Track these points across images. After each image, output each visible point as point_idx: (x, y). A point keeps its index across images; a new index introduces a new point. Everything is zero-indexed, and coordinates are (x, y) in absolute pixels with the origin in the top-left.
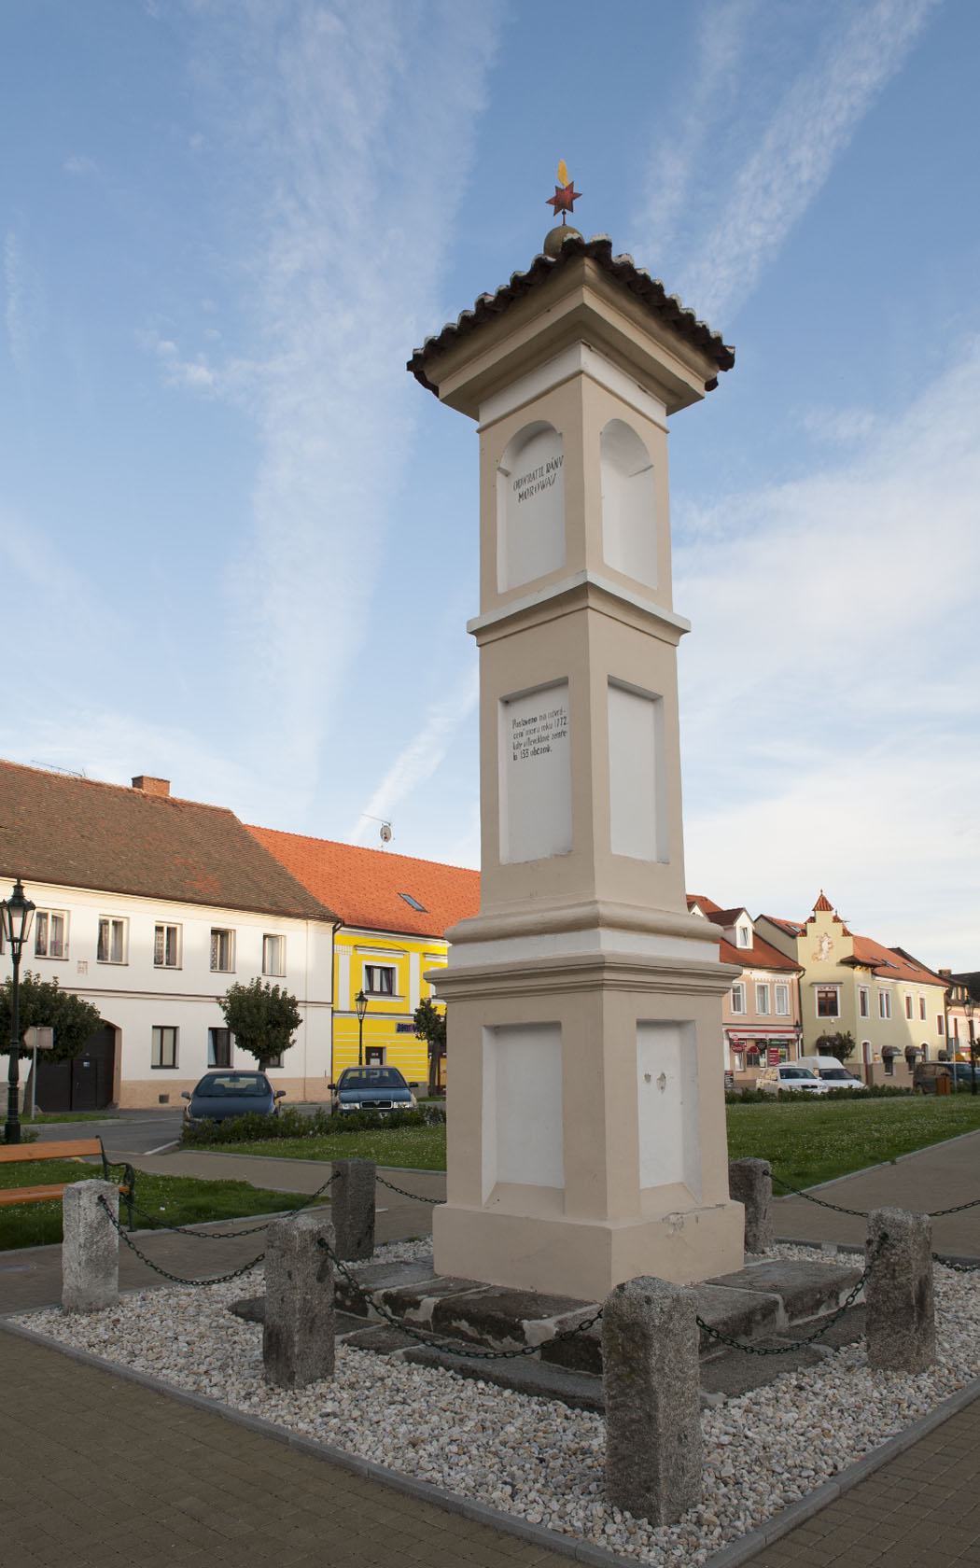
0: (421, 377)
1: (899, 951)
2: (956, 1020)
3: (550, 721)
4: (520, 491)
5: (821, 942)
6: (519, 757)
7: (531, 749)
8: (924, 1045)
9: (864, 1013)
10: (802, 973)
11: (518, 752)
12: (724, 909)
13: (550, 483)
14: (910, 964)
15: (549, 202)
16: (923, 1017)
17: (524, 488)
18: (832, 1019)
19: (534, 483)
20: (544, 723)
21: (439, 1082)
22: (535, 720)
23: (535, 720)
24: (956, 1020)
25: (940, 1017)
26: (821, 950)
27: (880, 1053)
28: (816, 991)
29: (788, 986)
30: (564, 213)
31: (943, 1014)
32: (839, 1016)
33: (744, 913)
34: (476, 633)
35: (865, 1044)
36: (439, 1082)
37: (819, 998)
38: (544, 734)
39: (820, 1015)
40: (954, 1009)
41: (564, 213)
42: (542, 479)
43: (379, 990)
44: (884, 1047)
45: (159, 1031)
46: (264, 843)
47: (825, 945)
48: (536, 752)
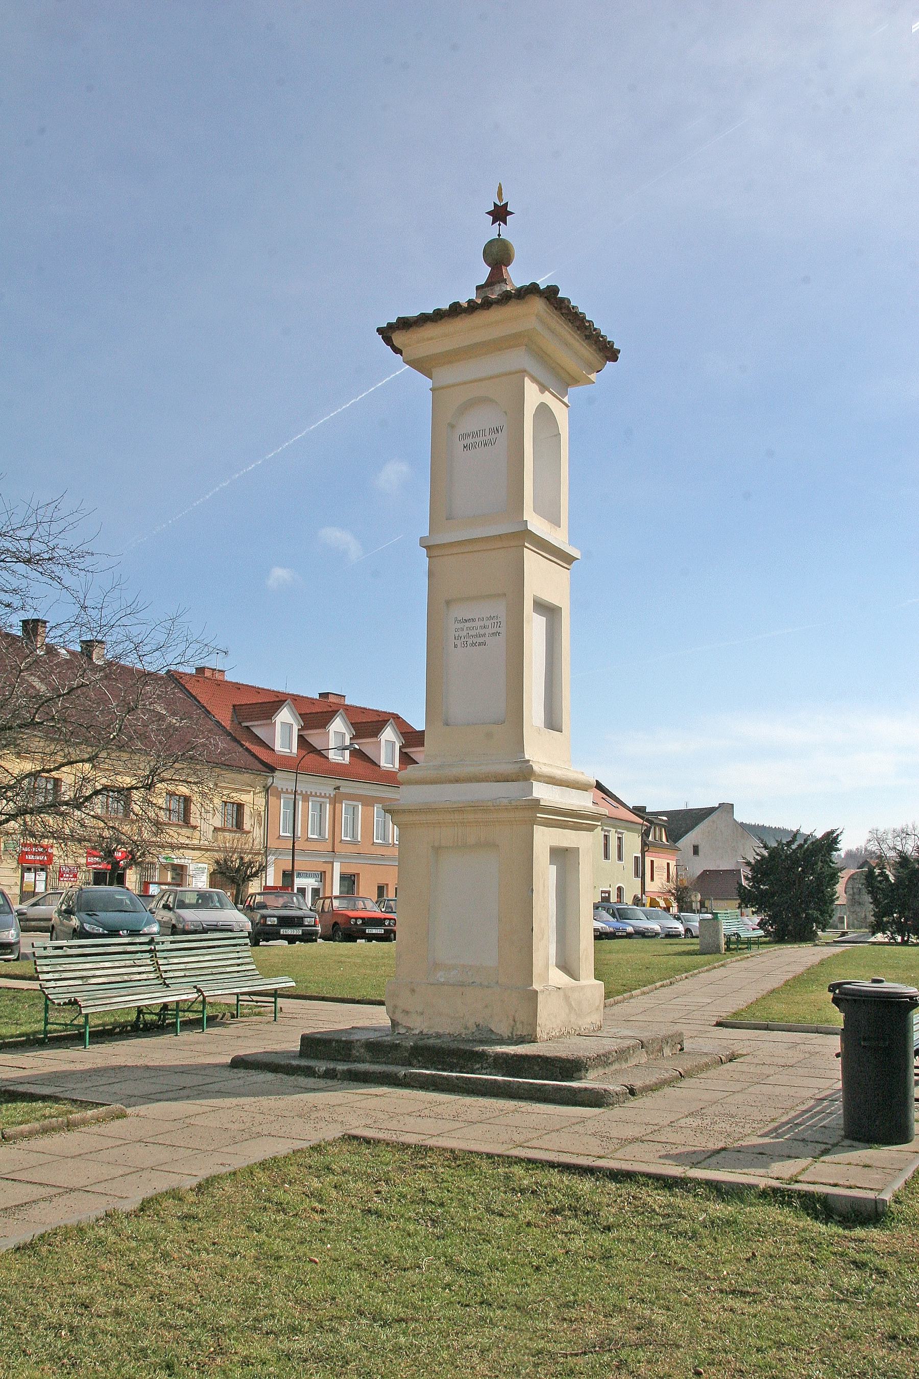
0: (388, 341)
2: (652, 862)
3: (488, 623)
4: (465, 442)
6: (459, 645)
7: (470, 641)
11: (458, 642)
13: (492, 443)
14: (608, 799)
16: (620, 858)
17: (469, 441)
19: (477, 440)
20: (482, 623)
21: (266, 884)
22: (474, 620)
23: (474, 620)
24: (652, 862)
25: (636, 858)
30: (499, 225)
34: (428, 548)
36: (266, 884)
38: (482, 632)
41: (499, 225)
42: (485, 438)
48: (473, 644)
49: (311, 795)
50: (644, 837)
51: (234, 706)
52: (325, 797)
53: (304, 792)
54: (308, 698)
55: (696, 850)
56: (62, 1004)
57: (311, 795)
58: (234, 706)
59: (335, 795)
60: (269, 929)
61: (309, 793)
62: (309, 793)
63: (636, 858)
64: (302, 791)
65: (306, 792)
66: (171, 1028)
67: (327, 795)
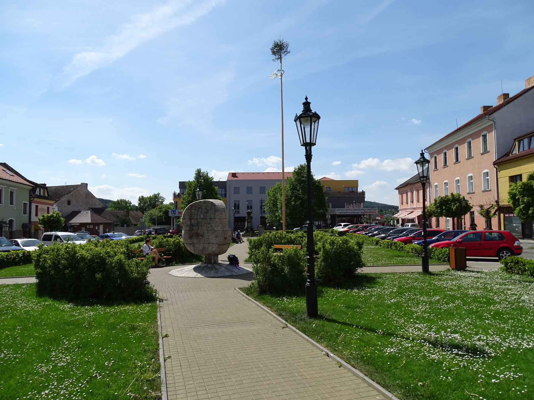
2: (37, 206)
8: (11, 221)
14: (8, 171)
24: (37, 206)
31: (28, 203)
40: (36, 199)
50: (31, 193)
55: (69, 203)
63: (25, 204)
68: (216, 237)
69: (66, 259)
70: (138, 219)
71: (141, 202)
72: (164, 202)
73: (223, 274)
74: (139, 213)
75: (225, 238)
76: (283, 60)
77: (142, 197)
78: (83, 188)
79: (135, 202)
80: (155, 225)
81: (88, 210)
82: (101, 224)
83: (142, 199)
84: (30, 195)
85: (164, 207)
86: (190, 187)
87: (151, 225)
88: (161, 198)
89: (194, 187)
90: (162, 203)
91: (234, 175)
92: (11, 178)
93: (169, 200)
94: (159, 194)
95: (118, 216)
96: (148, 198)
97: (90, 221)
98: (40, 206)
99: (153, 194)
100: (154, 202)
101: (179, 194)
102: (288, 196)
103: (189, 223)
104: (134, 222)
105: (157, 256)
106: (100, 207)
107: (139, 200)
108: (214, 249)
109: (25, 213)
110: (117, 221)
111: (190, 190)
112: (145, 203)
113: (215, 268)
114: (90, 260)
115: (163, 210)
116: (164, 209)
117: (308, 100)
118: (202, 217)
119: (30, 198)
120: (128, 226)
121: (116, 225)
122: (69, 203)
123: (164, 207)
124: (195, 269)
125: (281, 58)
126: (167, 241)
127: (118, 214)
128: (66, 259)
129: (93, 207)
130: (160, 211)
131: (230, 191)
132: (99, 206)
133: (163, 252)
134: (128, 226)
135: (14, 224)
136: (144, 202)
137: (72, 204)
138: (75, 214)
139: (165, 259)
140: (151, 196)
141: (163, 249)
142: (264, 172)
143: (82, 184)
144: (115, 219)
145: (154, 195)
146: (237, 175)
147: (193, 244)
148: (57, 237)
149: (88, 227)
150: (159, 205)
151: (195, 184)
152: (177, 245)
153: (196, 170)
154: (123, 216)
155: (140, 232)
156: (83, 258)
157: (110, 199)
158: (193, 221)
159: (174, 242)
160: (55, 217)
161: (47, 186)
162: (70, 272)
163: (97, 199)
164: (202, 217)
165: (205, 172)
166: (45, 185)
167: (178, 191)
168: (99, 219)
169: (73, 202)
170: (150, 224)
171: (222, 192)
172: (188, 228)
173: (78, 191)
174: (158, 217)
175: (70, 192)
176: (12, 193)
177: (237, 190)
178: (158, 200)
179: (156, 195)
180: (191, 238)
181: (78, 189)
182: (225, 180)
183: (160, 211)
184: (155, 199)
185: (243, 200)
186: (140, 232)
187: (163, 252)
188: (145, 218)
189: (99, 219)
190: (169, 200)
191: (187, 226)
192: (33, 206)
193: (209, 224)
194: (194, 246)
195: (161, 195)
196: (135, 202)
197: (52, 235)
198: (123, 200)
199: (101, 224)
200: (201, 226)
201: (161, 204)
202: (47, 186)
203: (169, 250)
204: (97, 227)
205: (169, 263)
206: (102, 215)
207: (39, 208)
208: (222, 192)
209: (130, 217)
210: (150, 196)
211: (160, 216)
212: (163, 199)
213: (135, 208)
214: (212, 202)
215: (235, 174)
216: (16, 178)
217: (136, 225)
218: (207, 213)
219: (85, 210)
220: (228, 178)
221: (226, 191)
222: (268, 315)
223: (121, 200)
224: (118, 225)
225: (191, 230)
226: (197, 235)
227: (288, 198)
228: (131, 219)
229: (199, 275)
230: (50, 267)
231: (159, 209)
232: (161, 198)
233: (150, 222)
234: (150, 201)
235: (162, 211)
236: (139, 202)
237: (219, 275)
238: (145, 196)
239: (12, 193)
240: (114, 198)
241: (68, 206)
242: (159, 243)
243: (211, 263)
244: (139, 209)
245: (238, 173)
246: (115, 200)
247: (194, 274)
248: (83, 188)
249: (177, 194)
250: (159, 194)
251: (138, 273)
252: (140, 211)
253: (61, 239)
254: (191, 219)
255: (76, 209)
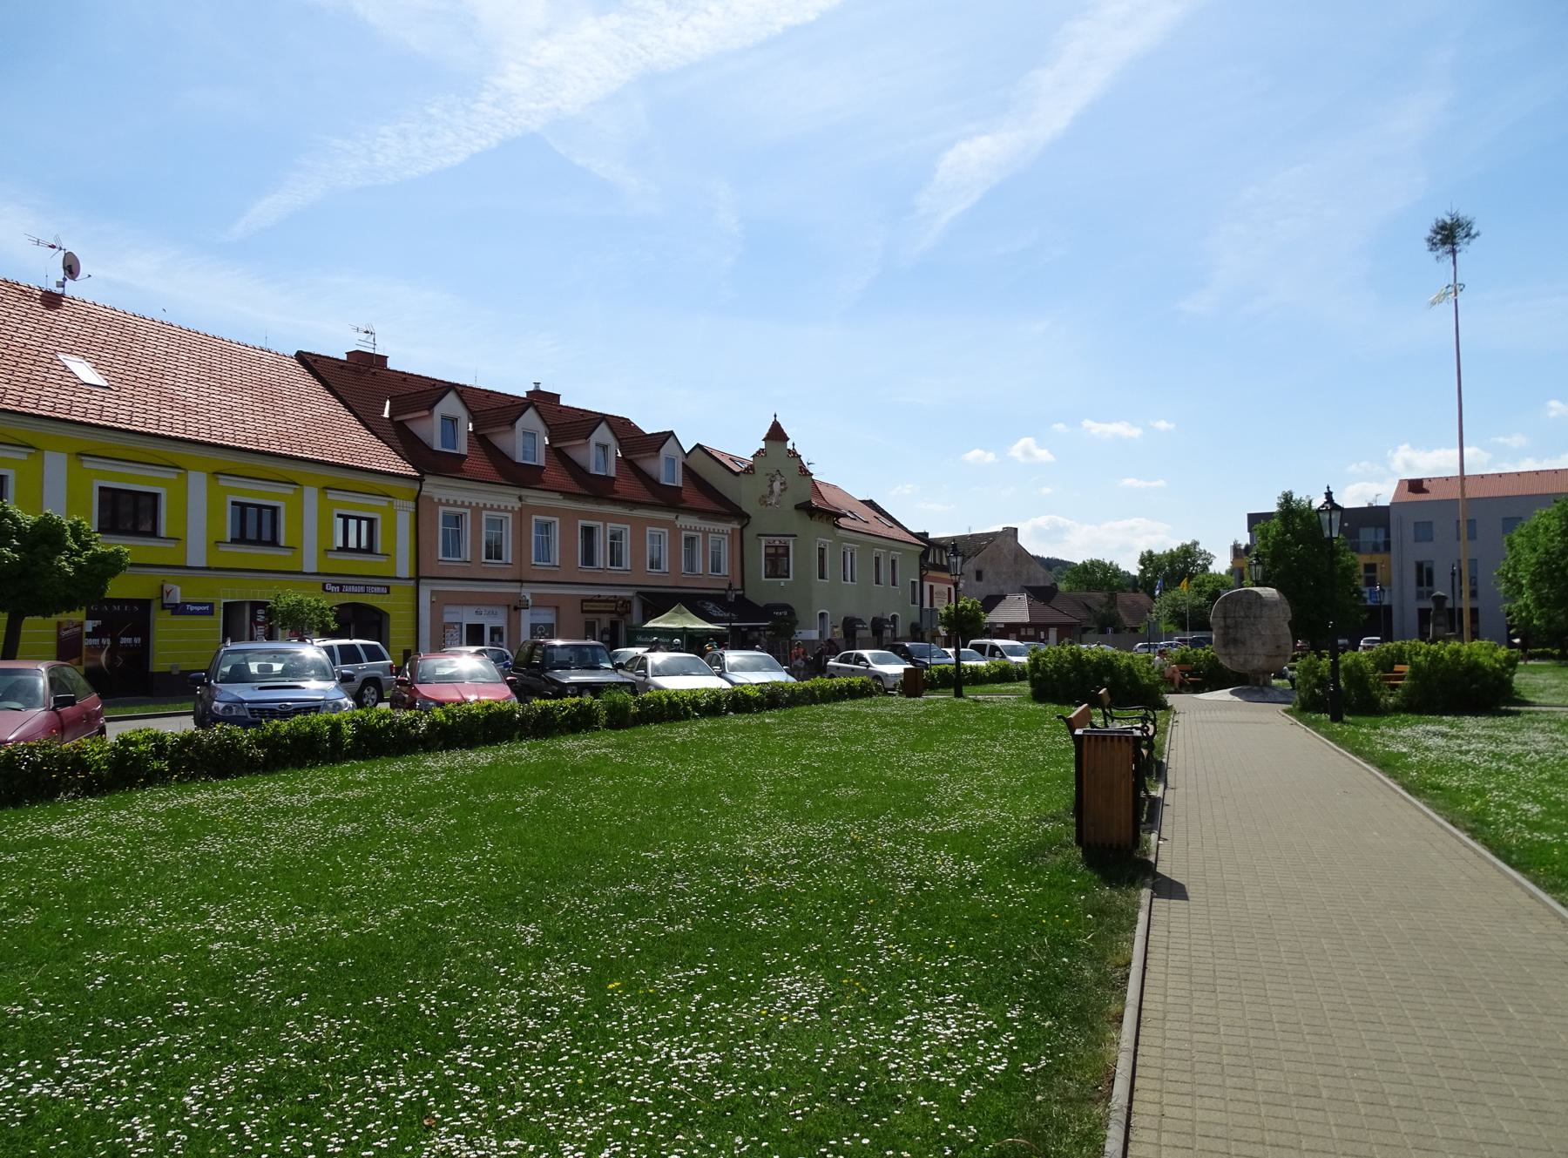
1: (870, 504)
2: (931, 587)
5: (772, 482)
8: (894, 617)
9: (822, 576)
10: (746, 521)
12: (648, 432)
14: (882, 519)
15: (776, 434)
18: (783, 581)
24: (931, 587)
26: (772, 492)
27: (840, 625)
28: (763, 545)
29: (726, 537)
31: (917, 580)
32: (791, 578)
33: (671, 439)
35: (822, 615)
37: (767, 555)
39: (102, 489)
40: (932, 574)
43: (355, 546)
44: (845, 618)
45: (422, 581)
46: (398, 445)
47: (777, 486)
49: (485, 507)
50: (923, 561)
51: (1430, 523)
52: (506, 510)
53: (474, 504)
54: (396, 372)
55: (979, 575)
56: (1053, 633)
57: (485, 507)
58: (1430, 523)
59: (521, 509)
60: (181, 709)
61: (481, 505)
62: (481, 505)
64: (477, 504)
65: (477, 504)
66: (870, 694)
67: (510, 508)
68: (1263, 644)
69: (1070, 663)
70: (1140, 613)
71: (1146, 568)
72: (1210, 567)
73: (1273, 700)
74: (1142, 598)
75: (1278, 647)
76: (1458, 255)
77: (1150, 553)
78: (1008, 539)
79: (1133, 568)
80: (1185, 630)
81: (1021, 592)
82: (1052, 625)
83: (1148, 559)
84: (921, 565)
85: (1209, 582)
86: (1266, 538)
87: (1175, 631)
88: (1201, 554)
89: (1273, 538)
90: (1205, 568)
91: (1416, 486)
92: (896, 536)
93: (1221, 564)
94: (1195, 544)
95: (1088, 608)
96: (1165, 555)
97: (1027, 620)
98: (937, 586)
99: (1179, 545)
100: (1182, 566)
101: (1247, 546)
102: (1553, 553)
103: (1222, 623)
104: (1128, 621)
105: (1178, 677)
106: (1048, 584)
107: (1142, 562)
108: (1261, 663)
109: (914, 603)
110: (1089, 620)
111: (1265, 545)
112: (1158, 569)
113: (1263, 692)
114: (1097, 663)
115: (1206, 589)
116: (1209, 588)
117: (1331, 490)
118: (1242, 614)
119: (921, 573)
120: (1116, 631)
121: (1085, 630)
122: (979, 575)
123: (1209, 582)
124: (1232, 693)
125: (1454, 252)
126: (1195, 654)
127: (1088, 602)
128: (1070, 663)
129: (1032, 584)
130: (1199, 593)
131: (1402, 534)
132: (1043, 579)
133: (1188, 672)
134: (1116, 631)
135: (899, 622)
136: (1154, 568)
137: (985, 578)
138: (991, 602)
139: (1191, 682)
140: (1175, 550)
141: (1188, 667)
142: (1520, 470)
143: (1007, 530)
144: (1083, 615)
145: (1182, 547)
146: (1425, 486)
147: (1229, 655)
148: (994, 648)
149: (1023, 633)
150: (1196, 574)
151: (1277, 531)
152: (1213, 661)
153: (1280, 495)
154: (1101, 606)
155: (1145, 646)
156: (1089, 660)
157: (1060, 557)
158: (1229, 620)
159: (1206, 656)
160: (970, 611)
161: (930, 537)
162: (1075, 676)
163: (1037, 558)
164: (1242, 614)
165: (1304, 498)
166: (926, 534)
167: (1244, 539)
168: (1048, 614)
169: (989, 573)
170: (1171, 627)
171: (1376, 537)
172: (1222, 631)
173: (997, 546)
174: (1193, 608)
175: (980, 550)
176: (893, 562)
177: (1424, 531)
178: (1195, 561)
179: (1187, 546)
180: (1225, 646)
181: (998, 542)
182: (1385, 500)
183: (1199, 593)
184: (1186, 558)
185: (1444, 555)
186: (1145, 646)
187: (1188, 672)
188: (1161, 606)
189: (1048, 614)
190: (1221, 564)
191: (1220, 628)
192: (927, 585)
193: (1253, 624)
194: (1230, 658)
195: (1201, 547)
196: (1133, 568)
197: (985, 645)
198: (1098, 561)
199: (1052, 625)
200: (1242, 628)
201: (1202, 572)
202: (930, 537)
203: (1198, 669)
204: (1042, 633)
205: (1198, 688)
206: (1052, 604)
207: (935, 590)
208: (1376, 537)
209: (1119, 610)
210: (1171, 550)
211: (1200, 606)
212: (1209, 559)
213: (1133, 583)
214: (1257, 593)
215: (1420, 482)
216: (896, 533)
217: (1134, 630)
218: (1250, 608)
219: (1014, 592)
220: (1394, 498)
221: (1388, 535)
222: (1517, 890)
223: (1092, 563)
224: (1091, 629)
225: (1226, 634)
226: (1235, 642)
227: (1551, 558)
228: (1121, 613)
229: (1237, 699)
230: (1051, 671)
231: (1195, 586)
232: (1201, 554)
233: (1170, 623)
234: (1171, 564)
235: (1205, 592)
236: (1142, 567)
237: (1267, 699)
238: (1158, 551)
239: (893, 562)
240: (1077, 554)
241: (977, 583)
242: (1182, 656)
243: (1258, 685)
244: (1141, 587)
245: (1430, 480)
246: (1079, 562)
247: (1230, 697)
248: (1008, 539)
249: (1243, 547)
250: (1195, 544)
251: (1150, 680)
252: (1146, 591)
253: (1002, 653)
254: (1225, 618)
255: (994, 591)
